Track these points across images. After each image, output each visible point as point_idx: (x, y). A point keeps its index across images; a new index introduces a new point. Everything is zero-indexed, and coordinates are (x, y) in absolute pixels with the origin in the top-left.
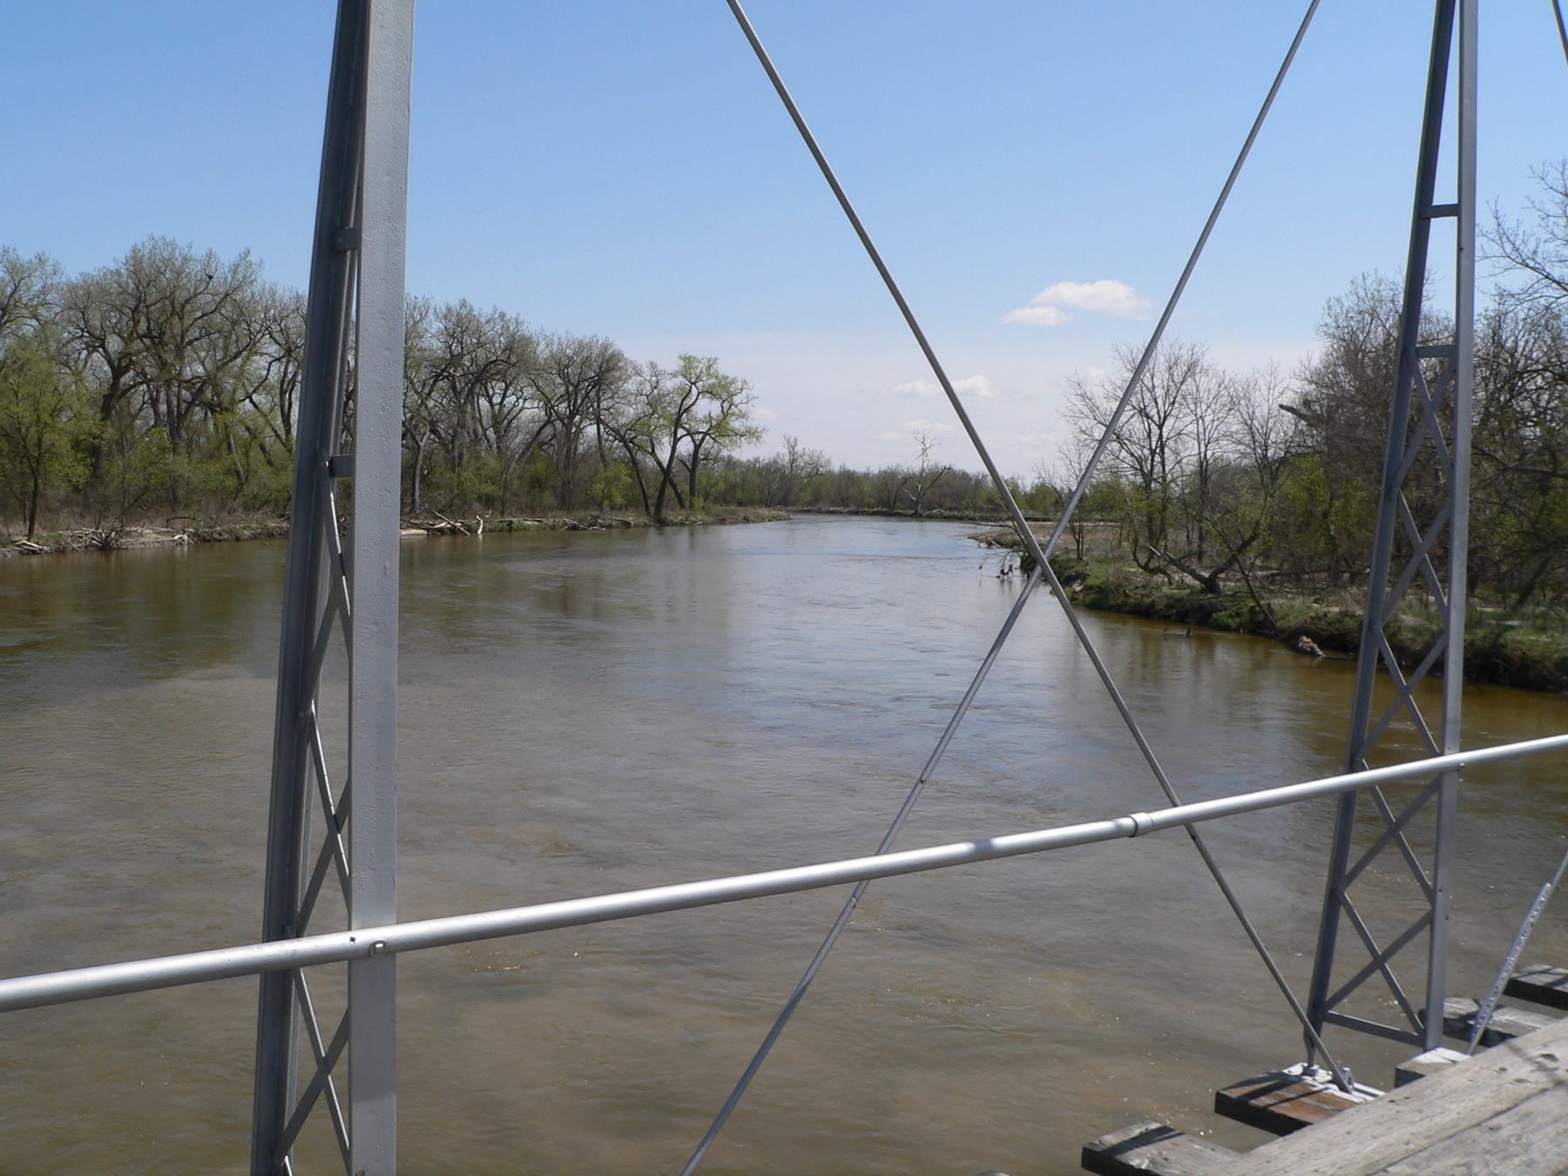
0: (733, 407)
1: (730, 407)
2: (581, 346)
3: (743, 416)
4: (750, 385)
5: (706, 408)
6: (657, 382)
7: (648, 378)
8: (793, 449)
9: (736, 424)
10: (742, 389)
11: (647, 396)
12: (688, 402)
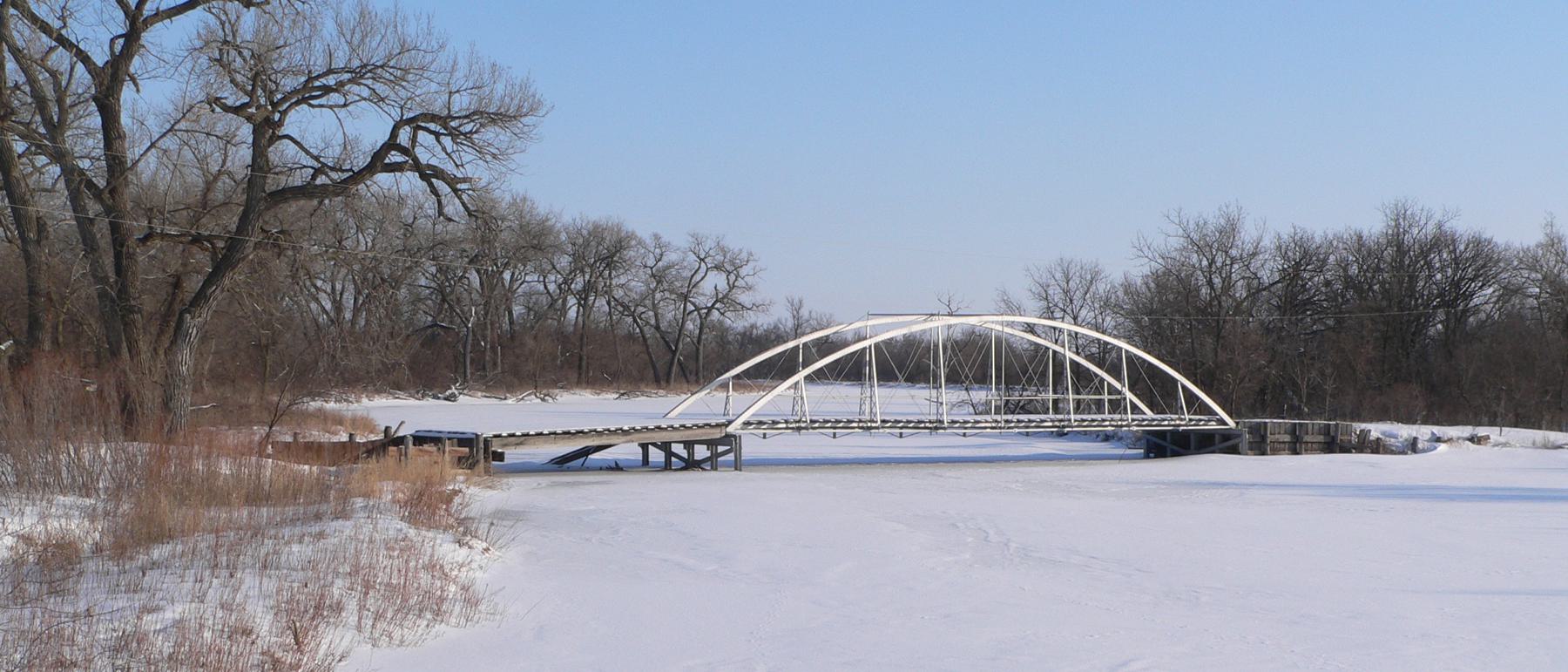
0: (739, 279)
1: (736, 280)
2: (596, 227)
3: (749, 288)
4: (756, 257)
5: (713, 283)
6: (662, 255)
7: (652, 249)
8: (798, 313)
9: (744, 298)
10: (748, 261)
11: (652, 268)
12: (697, 277)
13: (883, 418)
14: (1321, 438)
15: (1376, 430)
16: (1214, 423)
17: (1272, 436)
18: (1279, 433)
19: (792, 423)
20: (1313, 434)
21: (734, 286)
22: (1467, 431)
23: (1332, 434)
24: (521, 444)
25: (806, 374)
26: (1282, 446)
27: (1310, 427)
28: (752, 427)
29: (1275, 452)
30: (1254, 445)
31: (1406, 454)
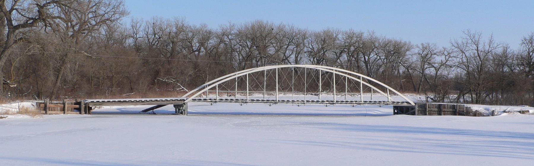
1: (449, 58)
13: (337, 100)
14: (451, 110)
15: (475, 107)
16: (406, 104)
17: (429, 109)
18: (433, 108)
19: (213, 100)
20: (447, 108)
21: (448, 60)
22: (519, 108)
23: (456, 108)
24: (101, 104)
25: (218, 84)
26: (434, 112)
27: (446, 106)
28: (196, 101)
29: (430, 114)
30: (422, 112)
31: (490, 116)
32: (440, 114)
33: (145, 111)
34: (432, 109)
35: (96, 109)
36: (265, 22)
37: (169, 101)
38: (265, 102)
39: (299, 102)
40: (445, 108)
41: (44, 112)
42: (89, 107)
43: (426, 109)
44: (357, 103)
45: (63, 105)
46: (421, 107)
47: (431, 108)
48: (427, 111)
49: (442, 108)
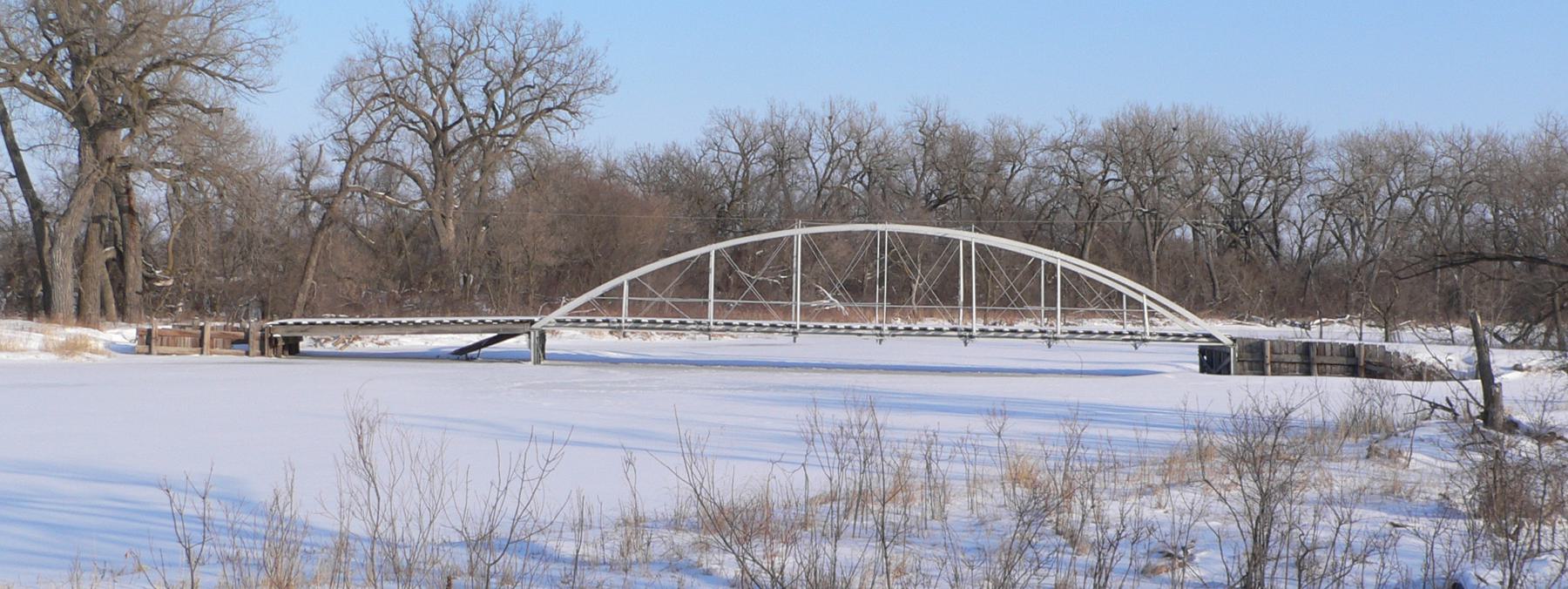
14: (1343, 360)
16: (1205, 340)
17: (1276, 356)
18: (1287, 353)
26: (1292, 367)
29: (1276, 372)
32: (1308, 373)
33: (463, 354)
34: (1282, 356)
35: (304, 345)
36: (1153, 109)
37: (490, 323)
38: (765, 329)
39: (866, 332)
40: (1325, 355)
41: (146, 348)
42: (271, 339)
43: (1263, 354)
44: (1046, 335)
45: (200, 331)
46: (1251, 352)
47: (1280, 354)
48: (1268, 360)
49: (1313, 353)
